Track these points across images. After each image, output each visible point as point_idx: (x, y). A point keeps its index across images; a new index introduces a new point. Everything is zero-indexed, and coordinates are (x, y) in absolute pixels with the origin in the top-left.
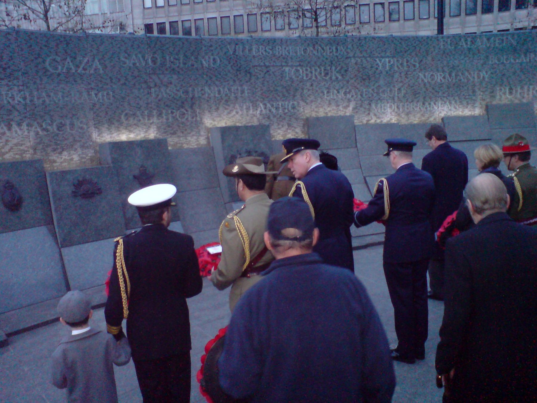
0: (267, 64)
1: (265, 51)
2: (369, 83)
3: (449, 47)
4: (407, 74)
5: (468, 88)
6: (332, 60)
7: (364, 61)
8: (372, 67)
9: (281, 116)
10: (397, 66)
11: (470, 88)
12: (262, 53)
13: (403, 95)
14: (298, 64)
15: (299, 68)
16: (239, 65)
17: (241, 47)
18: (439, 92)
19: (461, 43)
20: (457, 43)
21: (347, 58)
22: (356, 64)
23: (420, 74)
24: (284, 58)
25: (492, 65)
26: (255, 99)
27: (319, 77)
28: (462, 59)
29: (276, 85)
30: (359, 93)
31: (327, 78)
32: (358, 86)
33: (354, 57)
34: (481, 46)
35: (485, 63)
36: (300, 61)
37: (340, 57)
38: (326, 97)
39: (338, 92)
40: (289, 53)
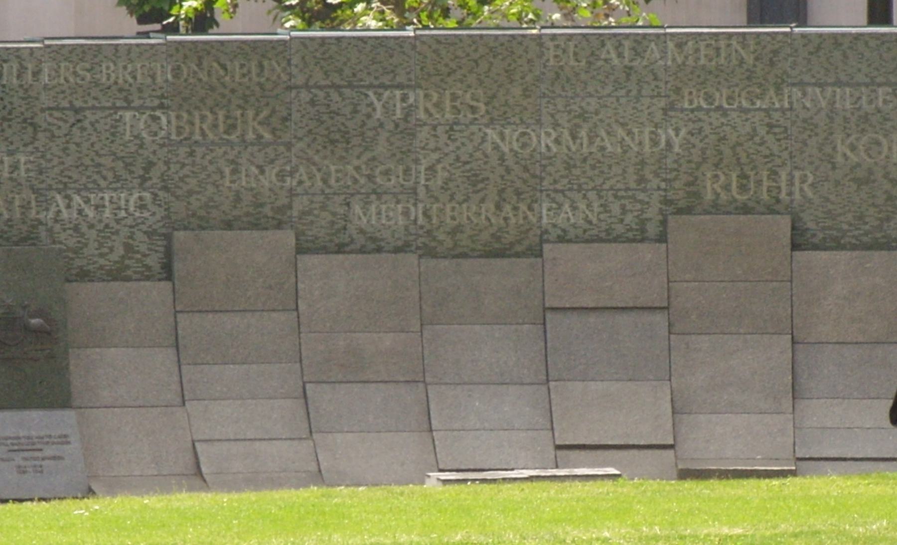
0: (78, 104)
1: (75, 73)
2: (347, 150)
3: (572, 63)
4: (452, 129)
5: (624, 171)
6: (248, 93)
7: (335, 96)
8: (355, 111)
9: (107, 226)
10: (426, 110)
11: (631, 170)
12: (66, 80)
13: (440, 183)
14: (156, 102)
15: (158, 113)
16: (9, 107)
17: (15, 66)
18: (542, 179)
19: (604, 50)
20: (593, 54)
21: (289, 88)
22: (312, 103)
23: (489, 131)
24: (121, 90)
25: (692, 111)
26: (43, 186)
27: (211, 136)
28: (609, 95)
29: (97, 153)
30: (318, 176)
31: (233, 137)
32: (316, 158)
33: (307, 86)
34: (661, 63)
35: (671, 107)
36: (162, 97)
37: (269, 86)
38: (228, 184)
39: (262, 172)
40: (135, 78)
